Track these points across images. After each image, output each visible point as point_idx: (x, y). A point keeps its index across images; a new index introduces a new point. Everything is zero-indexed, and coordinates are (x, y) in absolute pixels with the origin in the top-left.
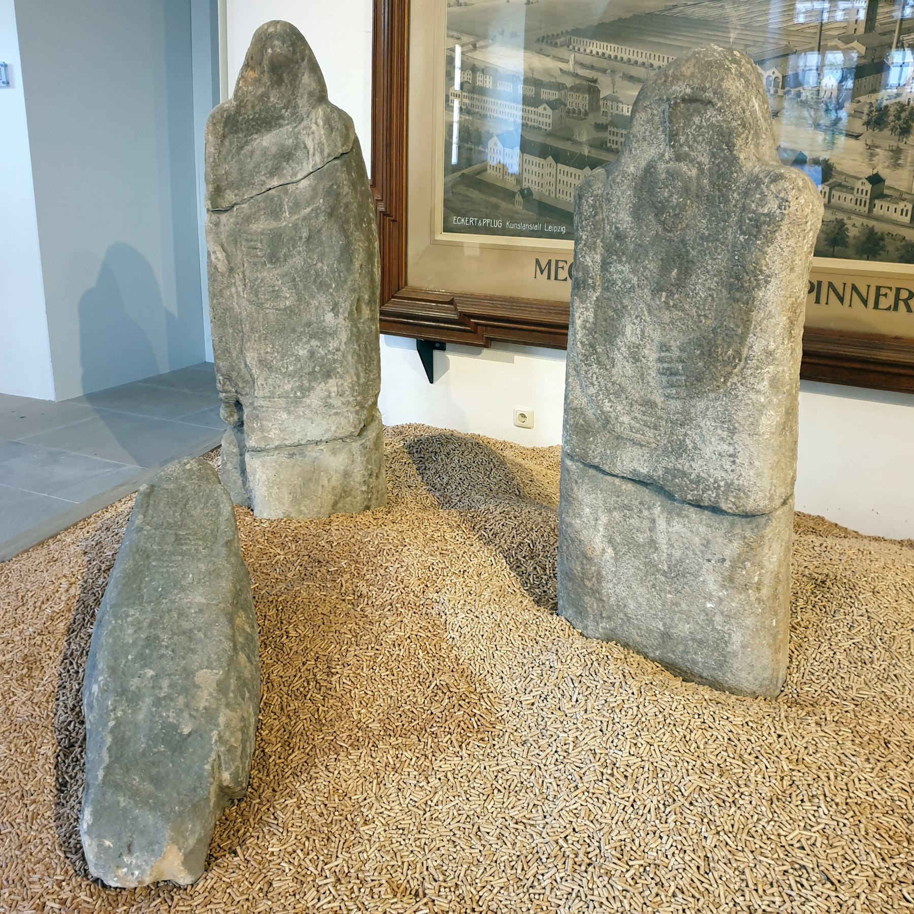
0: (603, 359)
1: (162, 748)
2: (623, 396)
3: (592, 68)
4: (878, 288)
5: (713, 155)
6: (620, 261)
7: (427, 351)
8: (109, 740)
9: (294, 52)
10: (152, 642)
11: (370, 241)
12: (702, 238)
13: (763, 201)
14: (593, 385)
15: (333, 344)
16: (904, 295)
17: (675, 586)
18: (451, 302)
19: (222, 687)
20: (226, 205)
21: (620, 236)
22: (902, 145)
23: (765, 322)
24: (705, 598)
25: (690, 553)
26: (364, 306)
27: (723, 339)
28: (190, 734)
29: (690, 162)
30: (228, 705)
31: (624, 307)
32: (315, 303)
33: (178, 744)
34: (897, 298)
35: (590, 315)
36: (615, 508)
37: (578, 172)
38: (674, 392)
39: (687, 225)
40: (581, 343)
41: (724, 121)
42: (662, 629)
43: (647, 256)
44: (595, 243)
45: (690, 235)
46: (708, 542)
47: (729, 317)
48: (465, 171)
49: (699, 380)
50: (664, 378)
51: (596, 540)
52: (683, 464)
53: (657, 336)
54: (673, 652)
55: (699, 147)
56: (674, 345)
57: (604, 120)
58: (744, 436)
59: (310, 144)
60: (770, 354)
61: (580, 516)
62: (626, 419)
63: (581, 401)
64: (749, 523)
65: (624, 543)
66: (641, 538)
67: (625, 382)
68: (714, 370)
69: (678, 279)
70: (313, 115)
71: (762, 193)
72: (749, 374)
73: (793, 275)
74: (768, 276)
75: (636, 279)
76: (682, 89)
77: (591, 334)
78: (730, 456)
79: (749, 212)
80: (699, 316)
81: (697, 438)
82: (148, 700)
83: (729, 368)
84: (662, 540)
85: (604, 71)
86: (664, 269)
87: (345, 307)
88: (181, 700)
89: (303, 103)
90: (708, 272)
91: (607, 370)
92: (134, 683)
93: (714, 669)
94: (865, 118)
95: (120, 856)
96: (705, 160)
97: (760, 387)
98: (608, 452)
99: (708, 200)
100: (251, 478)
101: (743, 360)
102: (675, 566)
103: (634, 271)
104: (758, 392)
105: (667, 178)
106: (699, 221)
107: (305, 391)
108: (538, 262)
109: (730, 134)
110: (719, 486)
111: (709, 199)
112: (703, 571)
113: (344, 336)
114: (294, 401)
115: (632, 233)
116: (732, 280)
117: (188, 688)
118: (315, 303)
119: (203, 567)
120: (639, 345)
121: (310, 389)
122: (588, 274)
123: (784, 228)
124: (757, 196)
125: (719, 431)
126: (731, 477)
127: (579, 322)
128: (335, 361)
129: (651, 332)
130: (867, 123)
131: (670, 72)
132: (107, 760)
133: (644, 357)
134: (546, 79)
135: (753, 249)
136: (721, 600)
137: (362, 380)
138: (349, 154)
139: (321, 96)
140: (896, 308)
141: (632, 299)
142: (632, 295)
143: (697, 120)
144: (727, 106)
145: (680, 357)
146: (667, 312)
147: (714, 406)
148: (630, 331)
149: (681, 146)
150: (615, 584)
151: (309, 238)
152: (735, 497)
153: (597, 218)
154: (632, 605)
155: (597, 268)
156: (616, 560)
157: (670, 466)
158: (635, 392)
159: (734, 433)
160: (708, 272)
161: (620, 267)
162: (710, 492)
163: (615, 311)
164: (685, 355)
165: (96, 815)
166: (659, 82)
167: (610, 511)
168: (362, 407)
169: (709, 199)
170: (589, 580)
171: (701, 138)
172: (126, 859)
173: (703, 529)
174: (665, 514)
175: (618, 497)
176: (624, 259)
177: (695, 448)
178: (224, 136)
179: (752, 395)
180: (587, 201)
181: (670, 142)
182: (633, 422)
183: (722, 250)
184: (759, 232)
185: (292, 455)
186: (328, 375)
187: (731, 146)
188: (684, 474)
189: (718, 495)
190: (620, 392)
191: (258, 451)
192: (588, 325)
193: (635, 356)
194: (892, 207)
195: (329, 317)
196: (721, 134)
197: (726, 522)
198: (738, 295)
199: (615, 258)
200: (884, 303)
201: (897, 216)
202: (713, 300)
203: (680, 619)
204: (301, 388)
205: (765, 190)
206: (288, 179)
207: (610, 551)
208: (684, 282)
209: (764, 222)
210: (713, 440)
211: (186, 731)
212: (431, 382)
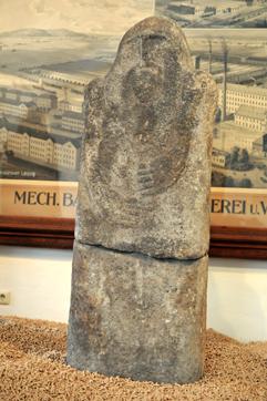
3: (53, 86)
4: (213, 201)
22: (217, 127)
31: (117, 146)
35: (96, 153)
37: (43, 141)
45: (155, 103)
52: (153, 233)
53: (136, 160)
57: (60, 113)
60: (199, 162)
65: (117, 292)
85: (60, 87)
86: (141, 122)
96: (162, 66)
103: (123, 125)
104: (194, 184)
108: (17, 193)
134: (25, 91)
136: (174, 316)
140: (222, 211)
148: (121, 159)
154: (120, 333)
156: (111, 305)
158: (124, 195)
163: (112, 149)
187: (176, 59)
188: (154, 240)
197: (177, 266)
207: (107, 300)
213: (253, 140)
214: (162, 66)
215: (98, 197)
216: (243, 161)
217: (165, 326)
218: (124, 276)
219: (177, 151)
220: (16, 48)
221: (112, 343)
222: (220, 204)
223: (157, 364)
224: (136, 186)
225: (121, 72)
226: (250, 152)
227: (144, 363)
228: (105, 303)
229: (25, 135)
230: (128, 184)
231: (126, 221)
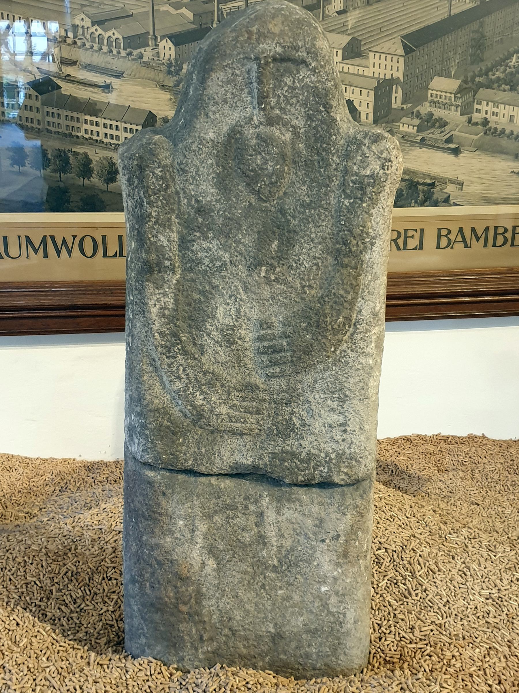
0: (190, 347)
2: (218, 384)
5: (309, 118)
6: (206, 238)
12: (303, 205)
13: (364, 162)
14: (180, 378)
17: (286, 579)
21: (201, 210)
23: (372, 283)
24: (319, 582)
25: (302, 539)
27: (332, 307)
29: (283, 125)
35: (170, 301)
36: (216, 512)
38: (278, 370)
39: (285, 193)
40: (161, 333)
41: (319, 82)
42: (273, 631)
43: (239, 229)
44: (169, 220)
45: (290, 204)
46: (321, 521)
47: (338, 284)
49: (307, 352)
50: (265, 358)
52: (292, 444)
54: (285, 652)
55: (293, 110)
56: (277, 321)
58: (355, 402)
61: (171, 532)
62: (223, 409)
64: (356, 490)
65: (226, 548)
66: (247, 537)
67: (218, 369)
68: (324, 340)
69: (280, 249)
71: (364, 154)
72: (359, 338)
74: (373, 238)
75: (227, 255)
76: (270, 48)
77: (172, 322)
78: (341, 425)
79: (353, 175)
80: (303, 287)
81: (304, 413)
83: (340, 336)
84: (271, 533)
86: (262, 242)
90: (312, 240)
91: (195, 359)
93: (328, 656)
96: (300, 123)
97: (368, 350)
98: (203, 450)
99: (306, 165)
101: (352, 326)
102: (286, 556)
103: (225, 247)
104: (367, 355)
105: (258, 144)
106: (299, 188)
109: (327, 95)
110: (331, 459)
111: (308, 164)
112: (318, 554)
115: (218, 206)
116: (338, 246)
120: (234, 326)
122: (163, 255)
124: (359, 158)
125: (329, 403)
126: (343, 446)
129: (247, 311)
131: (254, 29)
133: (240, 338)
135: (359, 212)
136: (335, 579)
141: (224, 277)
142: (224, 273)
143: (288, 80)
144: (322, 66)
145: (284, 333)
146: (267, 288)
147: (322, 378)
148: (222, 312)
149: (272, 108)
150: (218, 598)
152: (347, 467)
153: (169, 191)
154: (238, 615)
155: (175, 248)
157: (278, 449)
158: (232, 377)
159: (344, 402)
160: (312, 240)
162: (322, 468)
163: (202, 293)
164: (289, 330)
166: (241, 38)
167: (209, 517)
169: (308, 164)
170: (185, 603)
171: (294, 100)
173: (315, 509)
174: (274, 504)
175: (219, 497)
176: (211, 235)
177: (304, 425)
180: (154, 173)
181: (260, 104)
182: (231, 411)
183: (326, 216)
184: (364, 194)
188: (294, 455)
189: (330, 469)
190: (214, 381)
192: (166, 312)
193: (229, 339)
196: (317, 95)
198: (346, 260)
199: (198, 234)
202: (318, 268)
203: (293, 613)
205: (366, 151)
207: (211, 563)
208: (287, 254)
209: (369, 184)
210: (322, 412)
215: (179, 385)
218: (240, 521)
224: (250, 359)
225: (211, 135)
228: (208, 569)
230: (239, 360)
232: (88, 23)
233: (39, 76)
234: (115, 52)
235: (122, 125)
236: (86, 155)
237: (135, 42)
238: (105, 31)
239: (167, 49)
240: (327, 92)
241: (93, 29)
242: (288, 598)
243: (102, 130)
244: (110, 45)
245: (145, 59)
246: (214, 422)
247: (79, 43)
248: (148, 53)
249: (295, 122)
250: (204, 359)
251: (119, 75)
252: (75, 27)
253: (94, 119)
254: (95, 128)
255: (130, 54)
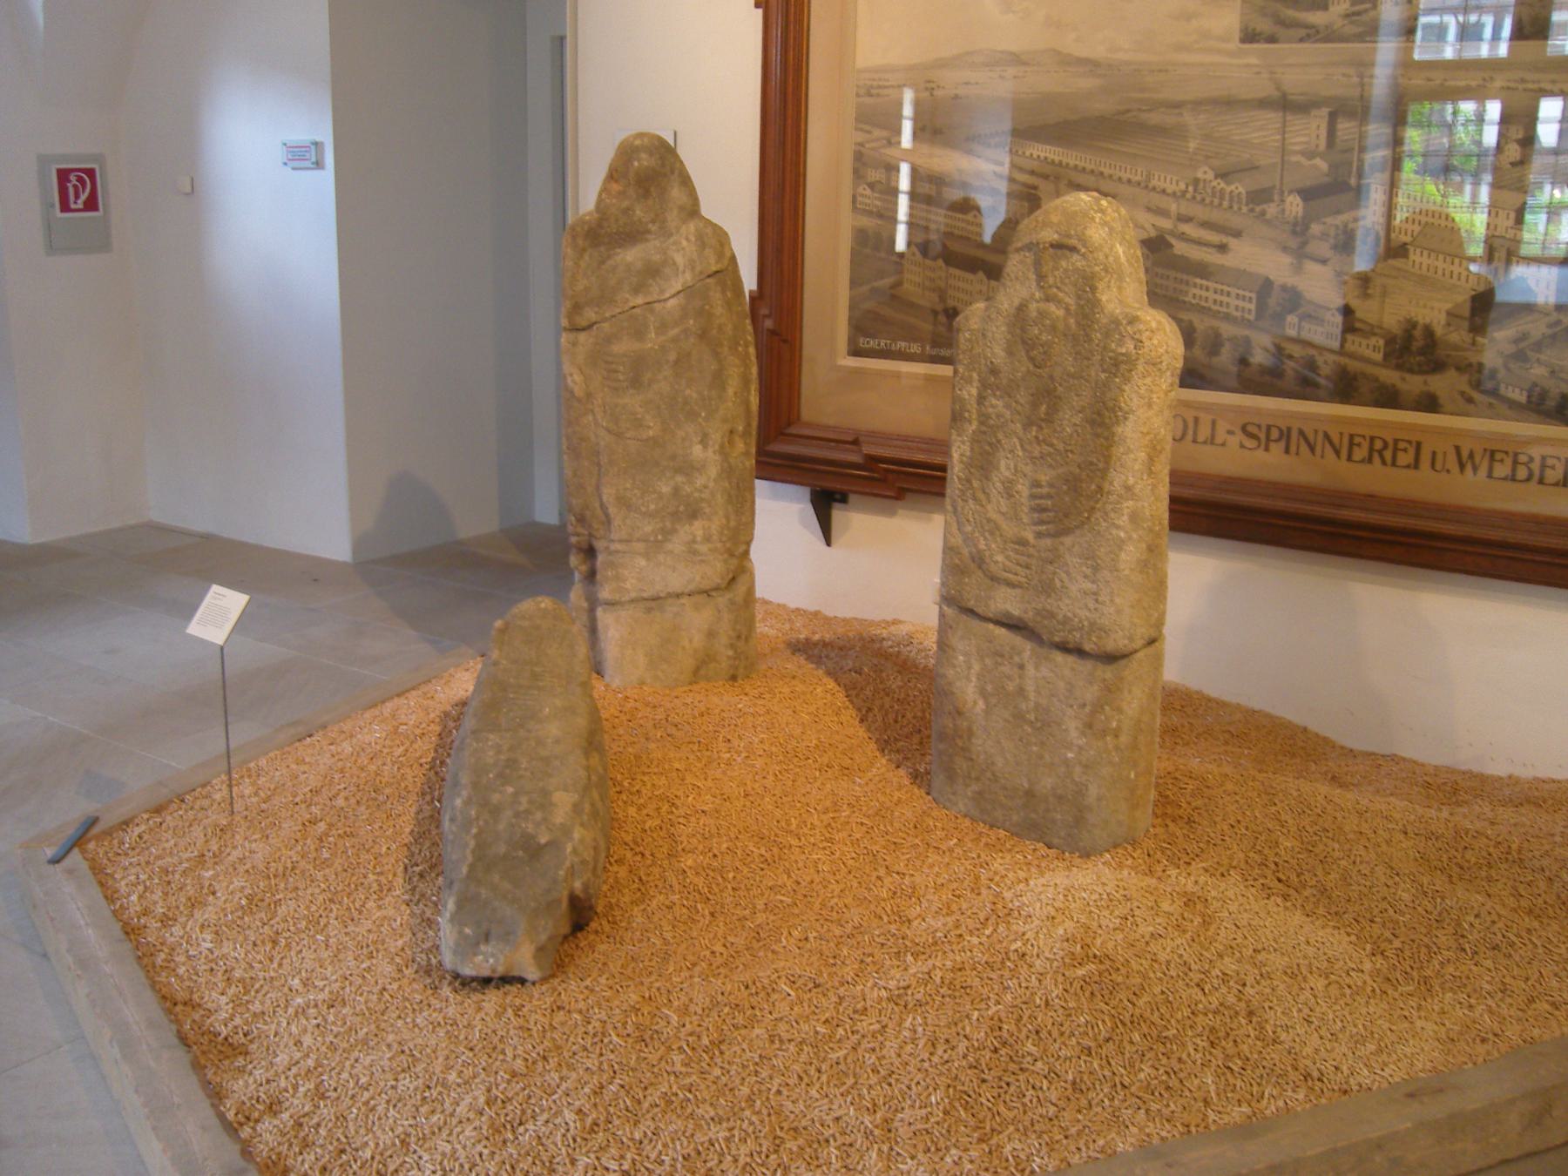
0: (980, 495)
1: (521, 853)
3: (1032, 173)
5: (1079, 297)
7: (825, 504)
8: (472, 843)
9: (663, 165)
10: (512, 763)
11: (747, 367)
13: (1121, 342)
15: (700, 481)
16: (1378, 445)
18: (856, 442)
19: (577, 808)
20: (584, 323)
21: (994, 371)
26: (737, 439)
28: (546, 845)
30: (582, 825)
32: (680, 433)
33: (534, 851)
34: (1371, 450)
35: (966, 448)
48: (876, 284)
51: (968, 691)
59: (680, 260)
60: (1128, 488)
62: (1000, 558)
63: (957, 540)
69: (1047, 414)
70: (683, 230)
73: (1151, 413)
82: (509, 813)
84: (1030, 688)
85: (1046, 177)
86: (1035, 406)
87: (716, 437)
88: (539, 816)
89: (673, 217)
92: (495, 798)
94: (1332, 241)
95: (478, 944)
96: (1070, 301)
100: (602, 636)
103: (1007, 406)
104: (1118, 527)
107: (668, 533)
113: (713, 471)
114: (654, 546)
117: (545, 804)
118: (680, 433)
119: (558, 702)
121: (674, 531)
123: (1140, 368)
127: (956, 456)
128: (702, 500)
130: (1335, 247)
132: (470, 859)
136: (1080, 748)
137: (733, 524)
138: (728, 272)
139: (693, 211)
148: (1004, 467)
151: (677, 362)
154: (1000, 762)
155: (973, 402)
157: (1040, 606)
158: (1009, 529)
161: (994, 401)
163: (990, 444)
165: (460, 905)
168: (732, 555)
172: (482, 948)
178: (584, 250)
179: (1114, 532)
185: (649, 610)
186: (694, 515)
187: (1093, 289)
188: (1052, 615)
190: (995, 529)
191: (611, 604)
193: (1009, 493)
194: (1364, 342)
195: (697, 450)
197: (1086, 666)
200: (1360, 454)
201: (1368, 353)
204: (663, 531)
206: (656, 297)
207: (981, 704)
211: (543, 841)
212: (828, 544)
213: (1449, 306)
214: (1070, 301)
216: (1422, 352)
217: (1066, 762)
218: (1006, 669)
219: (1092, 463)
220: (960, 92)
221: (989, 774)
222: (1366, 445)
223: (1054, 821)
226: (1439, 331)
227: (1033, 816)
229: (981, 275)
231: (1011, 576)
232: (1210, 175)
233: (1153, 234)
234: (1235, 207)
235: (1234, 291)
236: (1191, 322)
237: (1259, 197)
238: (1228, 183)
239: (1295, 205)
240: (1093, 276)
241: (1214, 183)
242: (1041, 757)
243: (1211, 295)
244: (1231, 200)
245: (1268, 216)
246: (993, 568)
247: (1199, 198)
248: (1271, 210)
249: (1067, 300)
250: (989, 507)
251: (1237, 234)
252: (1196, 181)
253: (1204, 282)
254: (1204, 294)
255: (1252, 210)
